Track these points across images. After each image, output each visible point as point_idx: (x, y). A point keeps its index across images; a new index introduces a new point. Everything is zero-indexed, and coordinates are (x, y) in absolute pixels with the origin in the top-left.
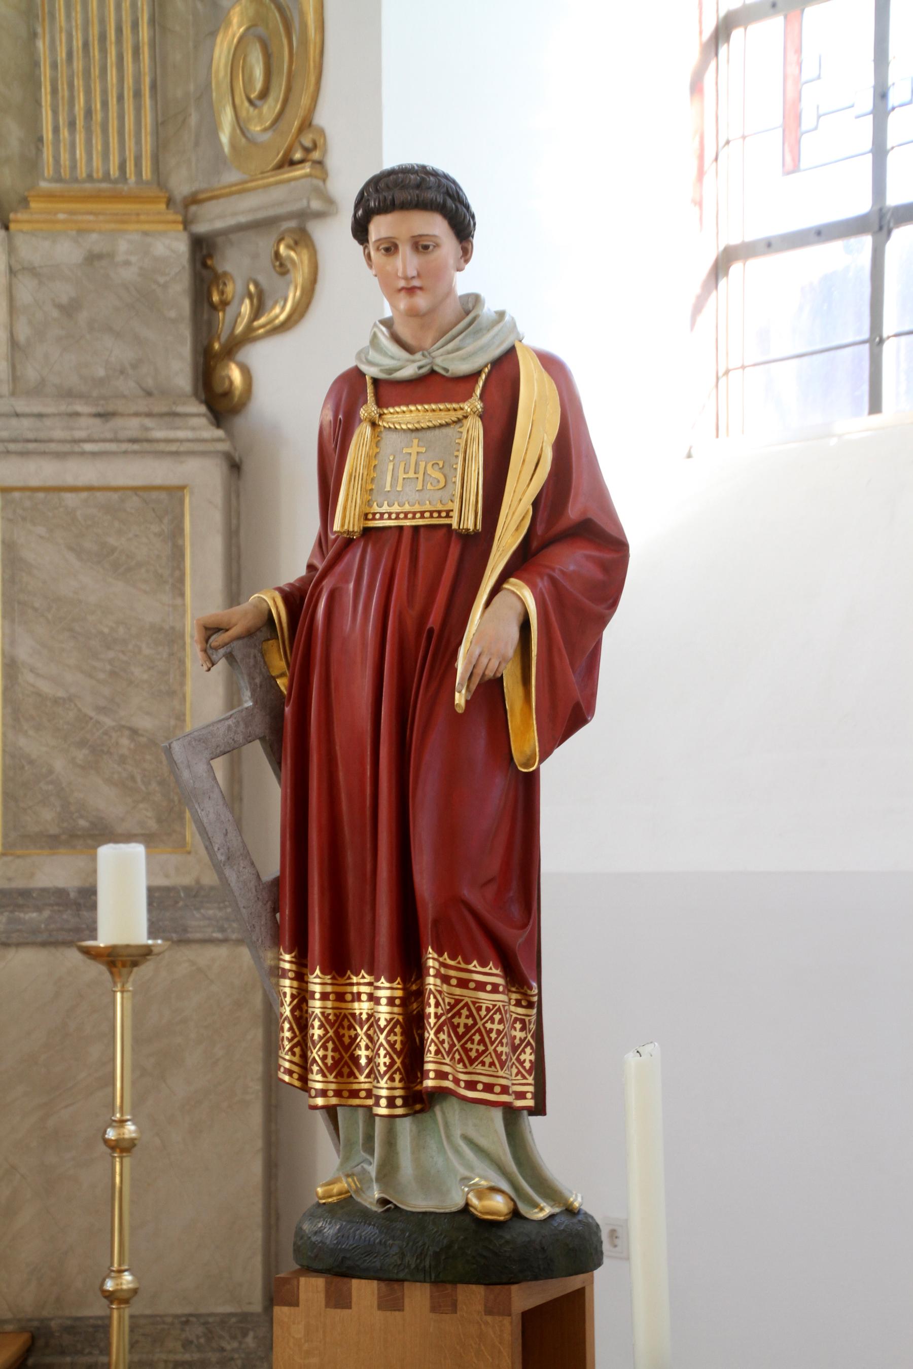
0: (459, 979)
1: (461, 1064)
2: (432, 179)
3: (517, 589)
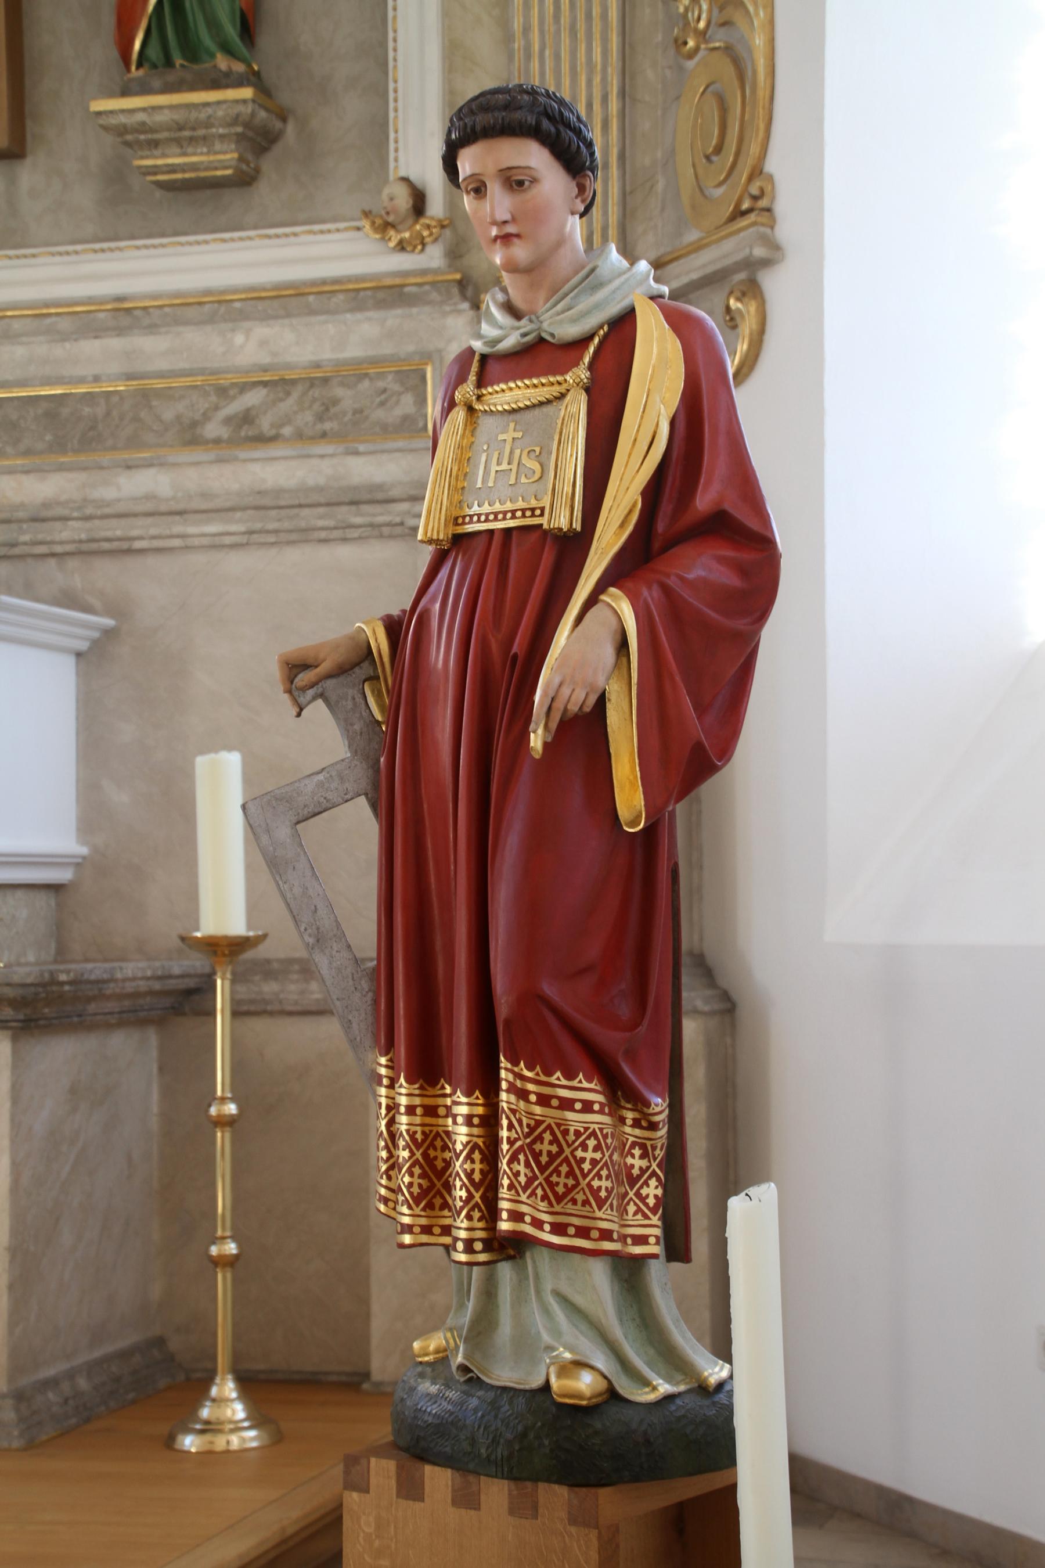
0: (539, 1095)
1: (546, 1202)
2: (526, 97)
3: (613, 601)
